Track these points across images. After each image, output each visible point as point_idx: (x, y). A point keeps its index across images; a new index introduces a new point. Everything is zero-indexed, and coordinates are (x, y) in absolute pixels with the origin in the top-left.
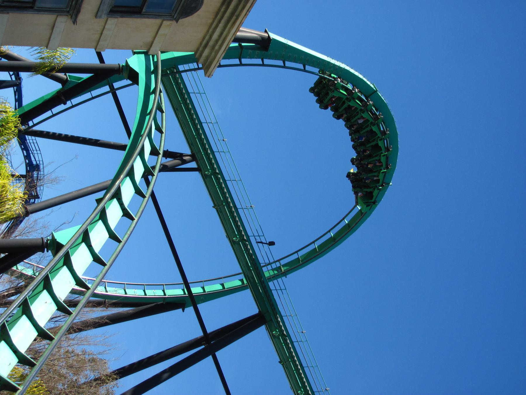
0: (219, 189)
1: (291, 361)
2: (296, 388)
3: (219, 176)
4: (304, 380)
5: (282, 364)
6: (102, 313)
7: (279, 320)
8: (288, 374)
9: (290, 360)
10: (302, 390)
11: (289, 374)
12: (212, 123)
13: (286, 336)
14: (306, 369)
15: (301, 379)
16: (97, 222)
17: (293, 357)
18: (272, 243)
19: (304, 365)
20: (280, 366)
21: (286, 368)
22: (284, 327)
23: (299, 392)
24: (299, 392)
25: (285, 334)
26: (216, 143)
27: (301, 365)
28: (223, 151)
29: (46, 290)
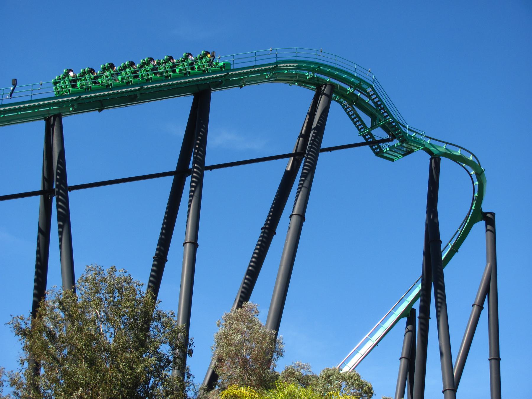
0: (253, 74)
1: (50, 108)
2: (67, 112)
3: (230, 73)
4: (41, 103)
5: (245, 85)
6: (51, 350)
7: (125, 91)
8: (36, 119)
9: (242, 77)
10: (265, 73)
11: (37, 118)
12: (3, 94)
13: (277, 66)
14: (258, 63)
15: (25, 109)
16: (434, 146)
17: (35, 106)
19: (28, 99)
20: (105, 111)
21: (10, 122)
22: (55, 100)
23: (267, 77)
24: (267, 77)
25: (76, 97)
26: (42, 93)
27: (253, 67)
28: (2, 95)
29: (486, 222)
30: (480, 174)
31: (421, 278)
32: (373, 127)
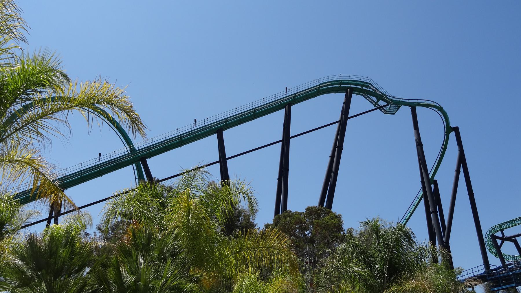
18: (195, 120)
30: (440, 109)
31: (423, 199)
32: (378, 101)
